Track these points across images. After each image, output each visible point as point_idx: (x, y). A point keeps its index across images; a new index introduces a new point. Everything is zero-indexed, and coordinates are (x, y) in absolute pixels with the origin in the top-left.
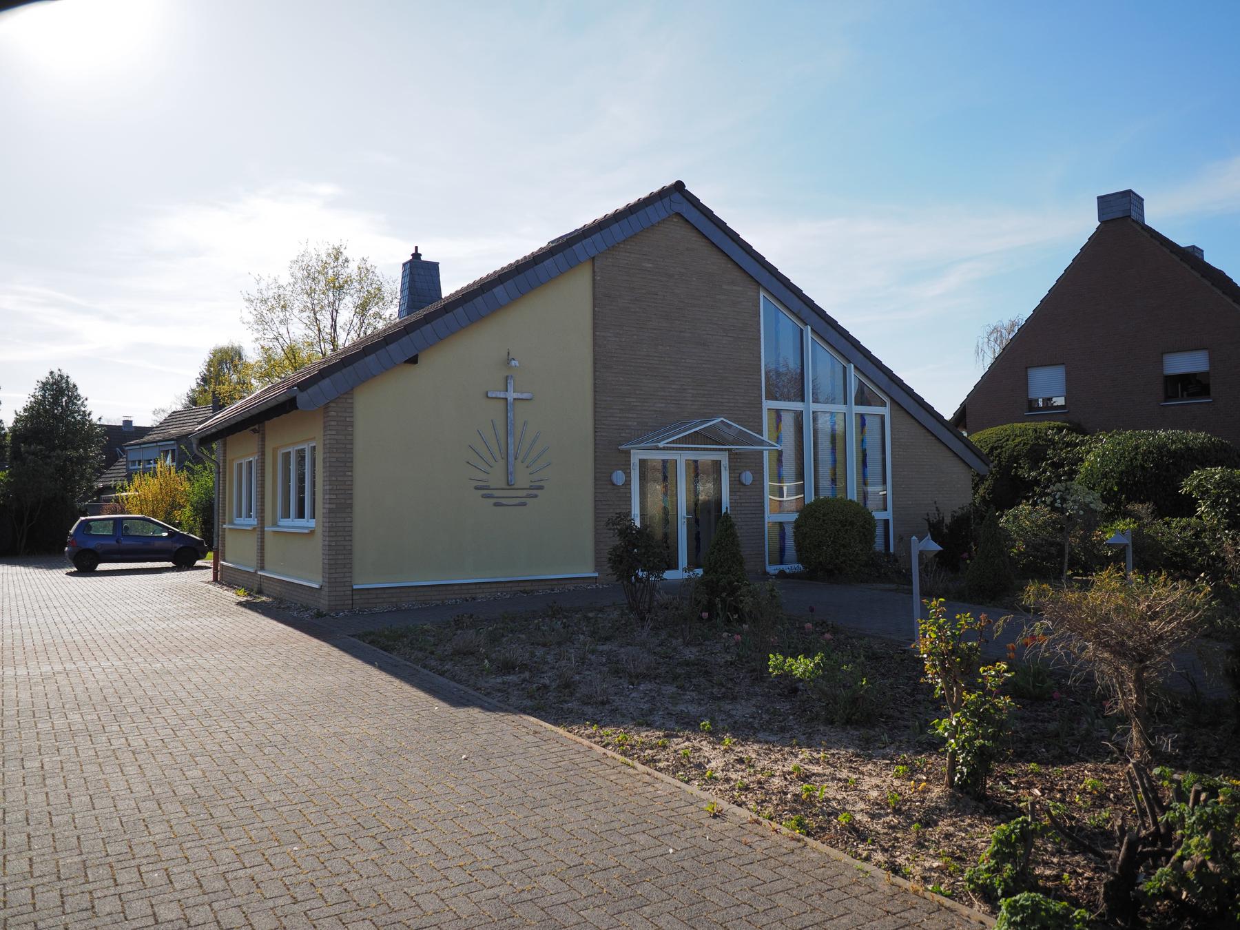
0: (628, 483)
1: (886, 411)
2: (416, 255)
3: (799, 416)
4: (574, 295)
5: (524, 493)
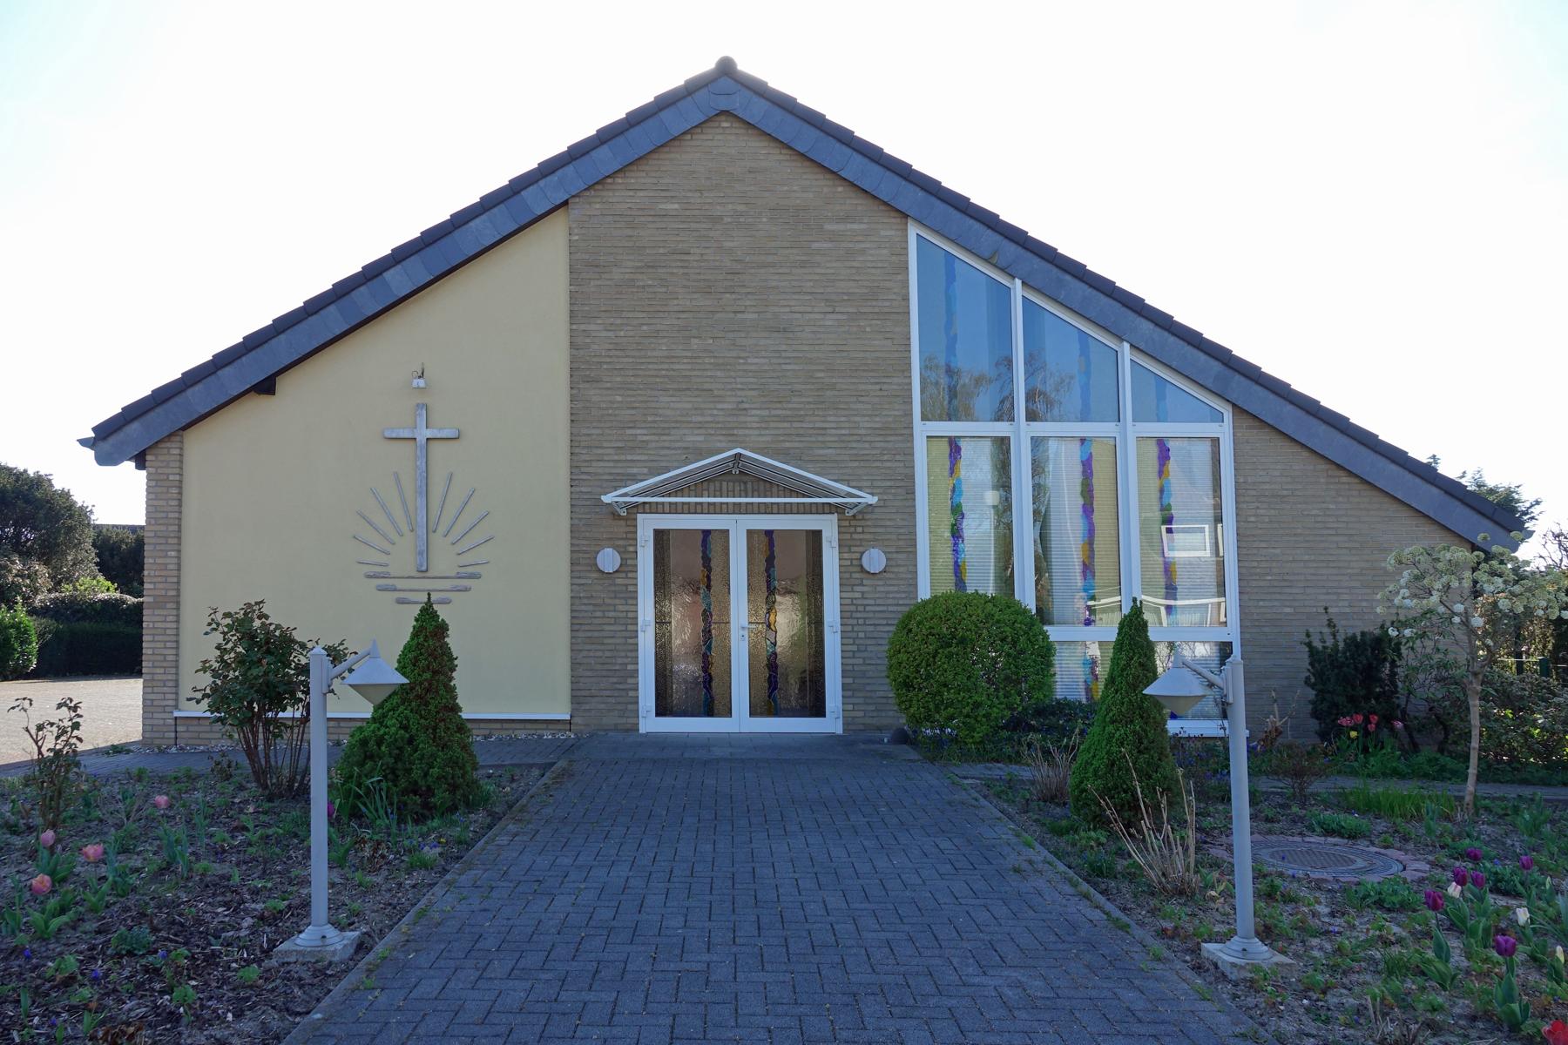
0: (628, 567)
1: (1224, 430)
2: (84, 442)
3: (1002, 444)
4: (541, 262)
5: (447, 584)
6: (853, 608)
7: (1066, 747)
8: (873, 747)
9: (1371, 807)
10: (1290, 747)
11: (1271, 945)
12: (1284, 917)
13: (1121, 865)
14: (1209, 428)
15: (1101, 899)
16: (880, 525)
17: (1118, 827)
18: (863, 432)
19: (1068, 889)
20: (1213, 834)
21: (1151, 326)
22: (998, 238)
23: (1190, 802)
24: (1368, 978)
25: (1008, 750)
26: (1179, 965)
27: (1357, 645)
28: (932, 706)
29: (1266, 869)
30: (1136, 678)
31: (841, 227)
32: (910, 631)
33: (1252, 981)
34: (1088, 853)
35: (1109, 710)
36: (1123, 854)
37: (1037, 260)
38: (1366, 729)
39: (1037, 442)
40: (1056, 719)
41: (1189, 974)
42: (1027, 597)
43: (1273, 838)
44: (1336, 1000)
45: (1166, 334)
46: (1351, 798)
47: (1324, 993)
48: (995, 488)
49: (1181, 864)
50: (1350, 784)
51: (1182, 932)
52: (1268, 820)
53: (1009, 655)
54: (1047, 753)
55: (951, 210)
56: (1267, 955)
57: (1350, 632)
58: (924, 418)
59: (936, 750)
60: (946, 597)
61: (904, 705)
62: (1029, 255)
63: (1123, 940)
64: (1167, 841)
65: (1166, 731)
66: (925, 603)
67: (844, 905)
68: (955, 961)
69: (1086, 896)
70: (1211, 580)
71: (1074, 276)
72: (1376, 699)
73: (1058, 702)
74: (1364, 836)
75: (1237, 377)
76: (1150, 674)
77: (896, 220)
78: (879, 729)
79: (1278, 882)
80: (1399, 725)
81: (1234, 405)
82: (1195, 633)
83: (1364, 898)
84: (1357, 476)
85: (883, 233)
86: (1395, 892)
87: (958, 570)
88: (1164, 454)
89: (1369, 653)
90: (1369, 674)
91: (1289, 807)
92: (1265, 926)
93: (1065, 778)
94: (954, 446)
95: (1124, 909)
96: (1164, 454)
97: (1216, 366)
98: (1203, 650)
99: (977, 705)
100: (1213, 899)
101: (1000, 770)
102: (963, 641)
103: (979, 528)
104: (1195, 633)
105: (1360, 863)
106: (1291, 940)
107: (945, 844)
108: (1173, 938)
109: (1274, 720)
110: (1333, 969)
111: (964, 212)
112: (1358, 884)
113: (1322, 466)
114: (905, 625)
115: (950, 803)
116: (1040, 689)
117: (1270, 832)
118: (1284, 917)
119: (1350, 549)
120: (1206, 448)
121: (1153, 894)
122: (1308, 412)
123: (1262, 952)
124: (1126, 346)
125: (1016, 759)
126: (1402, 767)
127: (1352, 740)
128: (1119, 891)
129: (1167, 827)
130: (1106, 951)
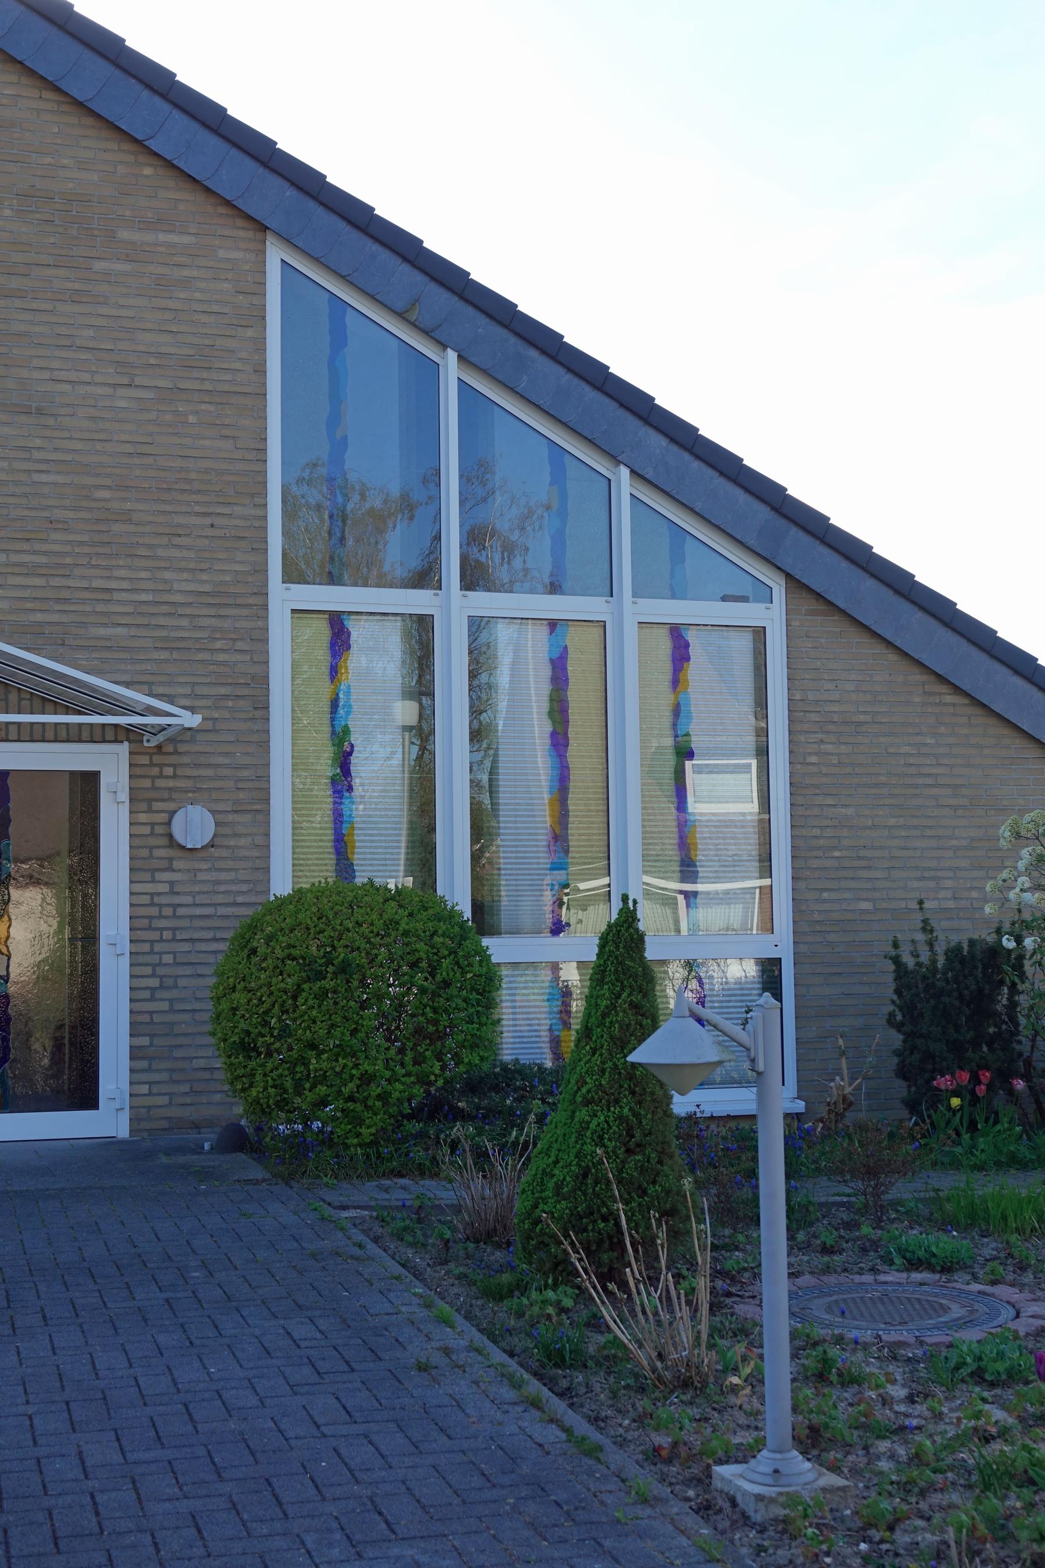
1: (772, 615)
6: (154, 911)
7: (515, 1144)
8: (182, 1159)
9: (975, 1220)
10: (862, 1127)
11: (819, 1460)
12: (839, 1408)
13: (595, 1341)
14: (748, 612)
15: (558, 1406)
16: (204, 762)
17: (588, 1281)
18: (179, 598)
19: (507, 1393)
20: (736, 1281)
21: (664, 442)
22: (419, 278)
23: (702, 1231)
24: (955, 1497)
25: (419, 1154)
26: (675, 1508)
27: (963, 961)
28: (289, 1084)
29: (818, 1332)
30: (625, 1027)
31: (149, 237)
32: (254, 951)
33: (785, 1521)
34: (541, 1328)
35: (581, 1082)
36: (596, 1323)
37: (484, 320)
38: (973, 1092)
39: (477, 626)
40: (498, 1095)
41: (691, 1521)
42: (456, 889)
43: (831, 1279)
44: (907, 1539)
45: (687, 456)
46: (948, 1207)
47: (891, 1528)
48: (409, 694)
49: (687, 1335)
50: (948, 1182)
51: (683, 1451)
52: (827, 1250)
53: (423, 991)
54: (481, 1156)
55: (341, 225)
56: (811, 1476)
57: (955, 938)
58: (293, 575)
59: (296, 1160)
60: (319, 892)
61: (241, 1082)
62: (470, 311)
63: (590, 1473)
64: (667, 1299)
65: (668, 1113)
66: (282, 902)
67: (117, 1457)
68: (309, 1540)
69: (535, 1404)
70: (750, 846)
71: (544, 352)
72: (990, 1045)
73: (505, 1067)
74: (965, 1267)
75: (794, 530)
76: (645, 1018)
77: (245, 234)
78: (197, 1126)
79: (834, 1352)
80: (1020, 1085)
81: (789, 577)
82: (721, 940)
83: (957, 1368)
84: (967, 695)
85: (221, 253)
86: (1001, 1355)
87: (341, 845)
88: (681, 655)
89: (979, 972)
90: (980, 1005)
91: (857, 1226)
92: (811, 1428)
93: (510, 1199)
94: (338, 631)
95: (595, 1420)
96: (681, 655)
97: (762, 512)
98: (741, 970)
99: (367, 1079)
100: (734, 1389)
101: (404, 1191)
102: (344, 969)
103: (380, 764)
104: (721, 940)
105: (957, 1311)
106: (847, 1447)
107: (301, 1330)
108: (669, 1461)
109: (842, 1085)
110: (906, 1487)
111: (363, 230)
112: (950, 1346)
113: (917, 677)
114: (245, 943)
115: (314, 1256)
116: (474, 1046)
117: (827, 1270)
118: (839, 1408)
119: (955, 808)
120: (743, 643)
121: (642, 1390)
122: (897, 592)
123: (804, 1473)
124: (625, 472)
125: (429, 1170)
126: (1024, 1151)
127: (954, 1112)
128: (589, 1389)
129: (667, 1278)
130: (562, 1496)
